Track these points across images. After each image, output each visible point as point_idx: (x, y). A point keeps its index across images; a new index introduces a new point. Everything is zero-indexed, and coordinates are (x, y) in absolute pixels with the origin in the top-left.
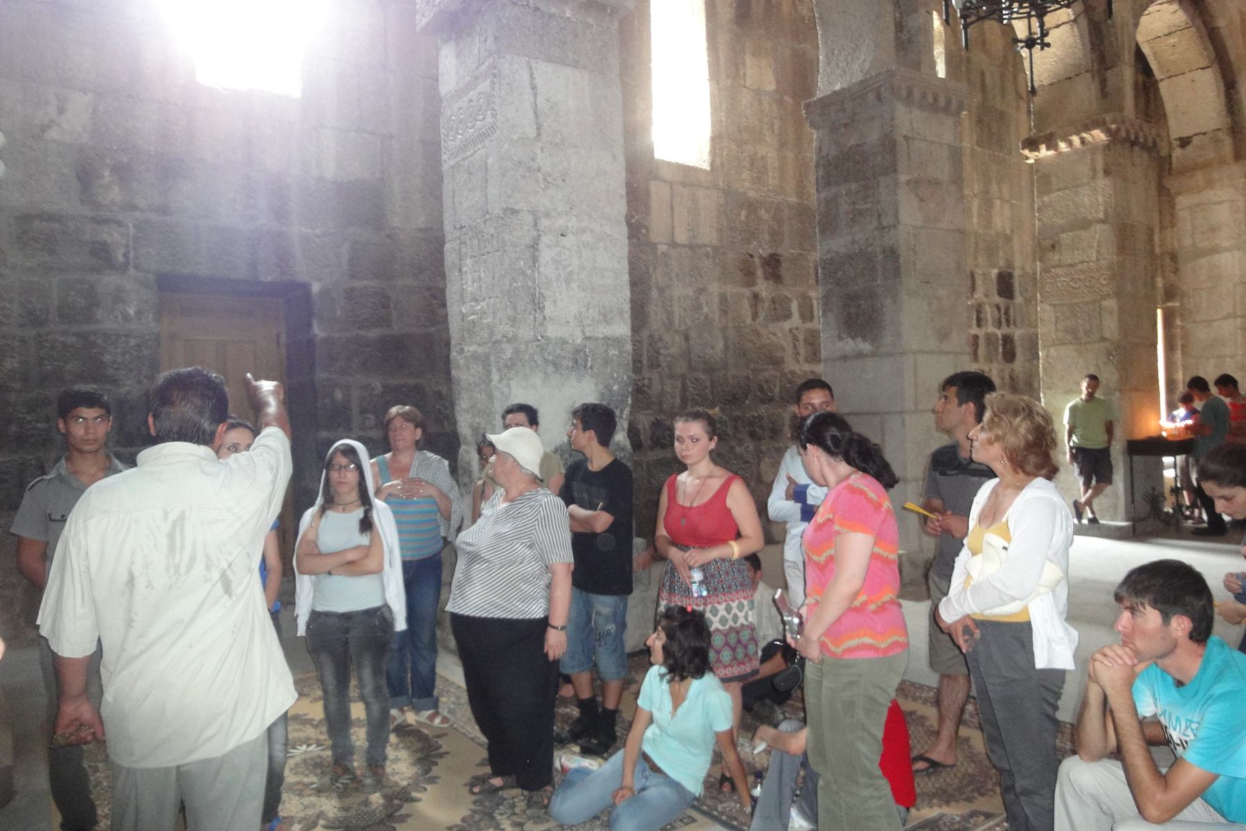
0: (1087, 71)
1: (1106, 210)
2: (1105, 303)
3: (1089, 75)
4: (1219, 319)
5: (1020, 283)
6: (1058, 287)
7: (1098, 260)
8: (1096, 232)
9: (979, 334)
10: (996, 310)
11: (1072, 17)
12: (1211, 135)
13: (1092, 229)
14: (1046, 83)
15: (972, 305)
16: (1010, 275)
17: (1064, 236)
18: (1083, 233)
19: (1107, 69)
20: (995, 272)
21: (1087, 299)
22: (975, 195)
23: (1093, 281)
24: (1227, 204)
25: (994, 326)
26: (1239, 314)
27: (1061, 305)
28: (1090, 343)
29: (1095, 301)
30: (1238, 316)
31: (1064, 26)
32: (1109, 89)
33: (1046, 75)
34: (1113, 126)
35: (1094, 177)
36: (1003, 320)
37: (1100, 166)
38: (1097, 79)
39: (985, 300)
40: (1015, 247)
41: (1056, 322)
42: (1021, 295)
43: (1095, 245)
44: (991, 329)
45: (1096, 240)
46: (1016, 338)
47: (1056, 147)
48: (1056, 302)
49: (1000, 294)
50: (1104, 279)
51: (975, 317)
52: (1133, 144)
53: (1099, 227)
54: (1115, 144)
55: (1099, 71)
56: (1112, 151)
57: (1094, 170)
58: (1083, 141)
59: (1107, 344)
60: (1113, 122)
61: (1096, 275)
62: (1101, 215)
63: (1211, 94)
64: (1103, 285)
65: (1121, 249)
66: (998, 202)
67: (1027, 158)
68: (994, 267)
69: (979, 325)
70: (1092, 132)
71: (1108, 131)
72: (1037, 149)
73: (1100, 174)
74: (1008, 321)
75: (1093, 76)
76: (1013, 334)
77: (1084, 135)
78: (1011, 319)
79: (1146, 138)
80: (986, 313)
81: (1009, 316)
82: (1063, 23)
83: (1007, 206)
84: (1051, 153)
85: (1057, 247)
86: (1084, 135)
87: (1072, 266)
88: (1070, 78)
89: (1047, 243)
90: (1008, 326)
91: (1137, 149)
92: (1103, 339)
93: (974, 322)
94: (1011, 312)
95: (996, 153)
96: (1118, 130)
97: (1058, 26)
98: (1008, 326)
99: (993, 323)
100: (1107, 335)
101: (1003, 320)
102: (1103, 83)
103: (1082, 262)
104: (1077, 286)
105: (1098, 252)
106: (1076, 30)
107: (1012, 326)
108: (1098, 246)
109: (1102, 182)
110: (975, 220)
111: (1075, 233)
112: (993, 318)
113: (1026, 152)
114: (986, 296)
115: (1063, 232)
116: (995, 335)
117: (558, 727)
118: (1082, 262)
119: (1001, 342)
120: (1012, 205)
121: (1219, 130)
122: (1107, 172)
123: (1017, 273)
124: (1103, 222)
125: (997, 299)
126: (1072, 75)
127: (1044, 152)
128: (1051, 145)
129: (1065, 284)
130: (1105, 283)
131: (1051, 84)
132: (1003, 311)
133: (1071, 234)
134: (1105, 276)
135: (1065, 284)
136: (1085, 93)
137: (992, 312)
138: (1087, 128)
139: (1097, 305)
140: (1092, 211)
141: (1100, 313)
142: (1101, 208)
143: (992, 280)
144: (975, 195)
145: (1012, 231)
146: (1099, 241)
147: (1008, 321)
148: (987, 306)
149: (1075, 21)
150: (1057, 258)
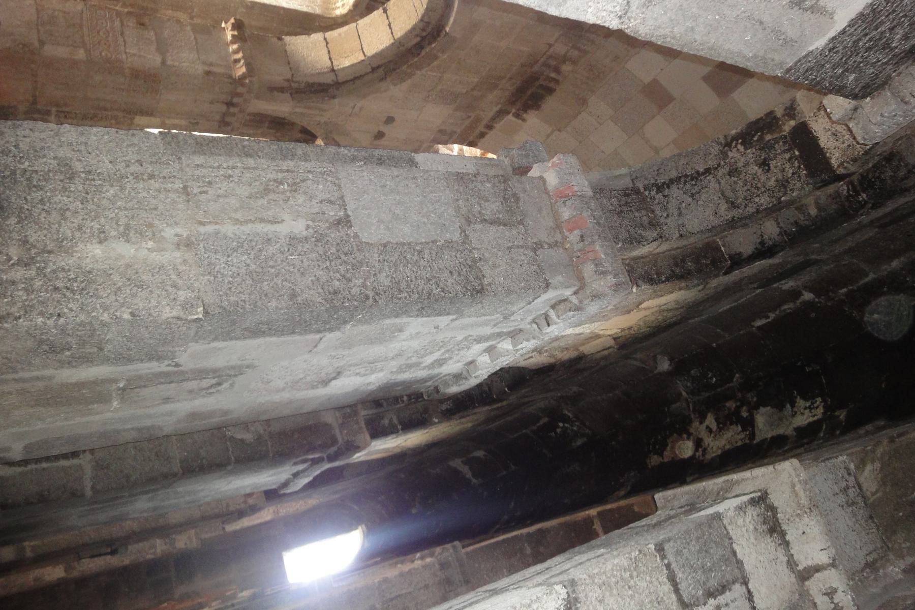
0: (293, 75)
3: (289, 76)
11: (336, 68)
14: (288, 48)
17: (152, 33)
18: (153, 48)
19: (291, 94)
29: (83, 43)
31: (330, 62)
32: (275, 93)
33: (293, 48)
34: (247, 81)
35: (204, 63)
37: (214, 69)
38: (285, 84)
45: (145, 55)
47: (233, 42)
52: (230, 104)
53: (159, 59)
54: (231, 84)
55: (290, 88)
56: (226, 80)
57: (211, 64)
58: (237, 61)
60: (250, 82)
61: (111, 49)
64: (101, 54)
65: (136, 74)
67: (226, 23)
70: (244, 67)
71: (243, 77)
72: (233, 29)
73: (207, 68)
75: (287, 80)
77: (242, 61)
79: (234, 115)
82: (332, 63)
84: (229, 38)
86: (242, 61)
87: (122, 34)
88: (289, 64)
89: (146, 20)
91: (224, 108)
92: (42, 43)
96: (243, 85)
97: (330, 58)
100: (46, 47)
102: (282, 90)
103: (124, 41)
105: (134, 55)
106: (326, 70)
109: (200, 69)
113: (232, 20)
117: (876, 118)
122: (208, 73)
124: (164, 62)
126: (291, 65)
127: (229, 35)
128: (235, 39)
131: (286, 51)
136: (277, 74)
138: (247, 64)
146: (145, 57)
149: (333, 70)
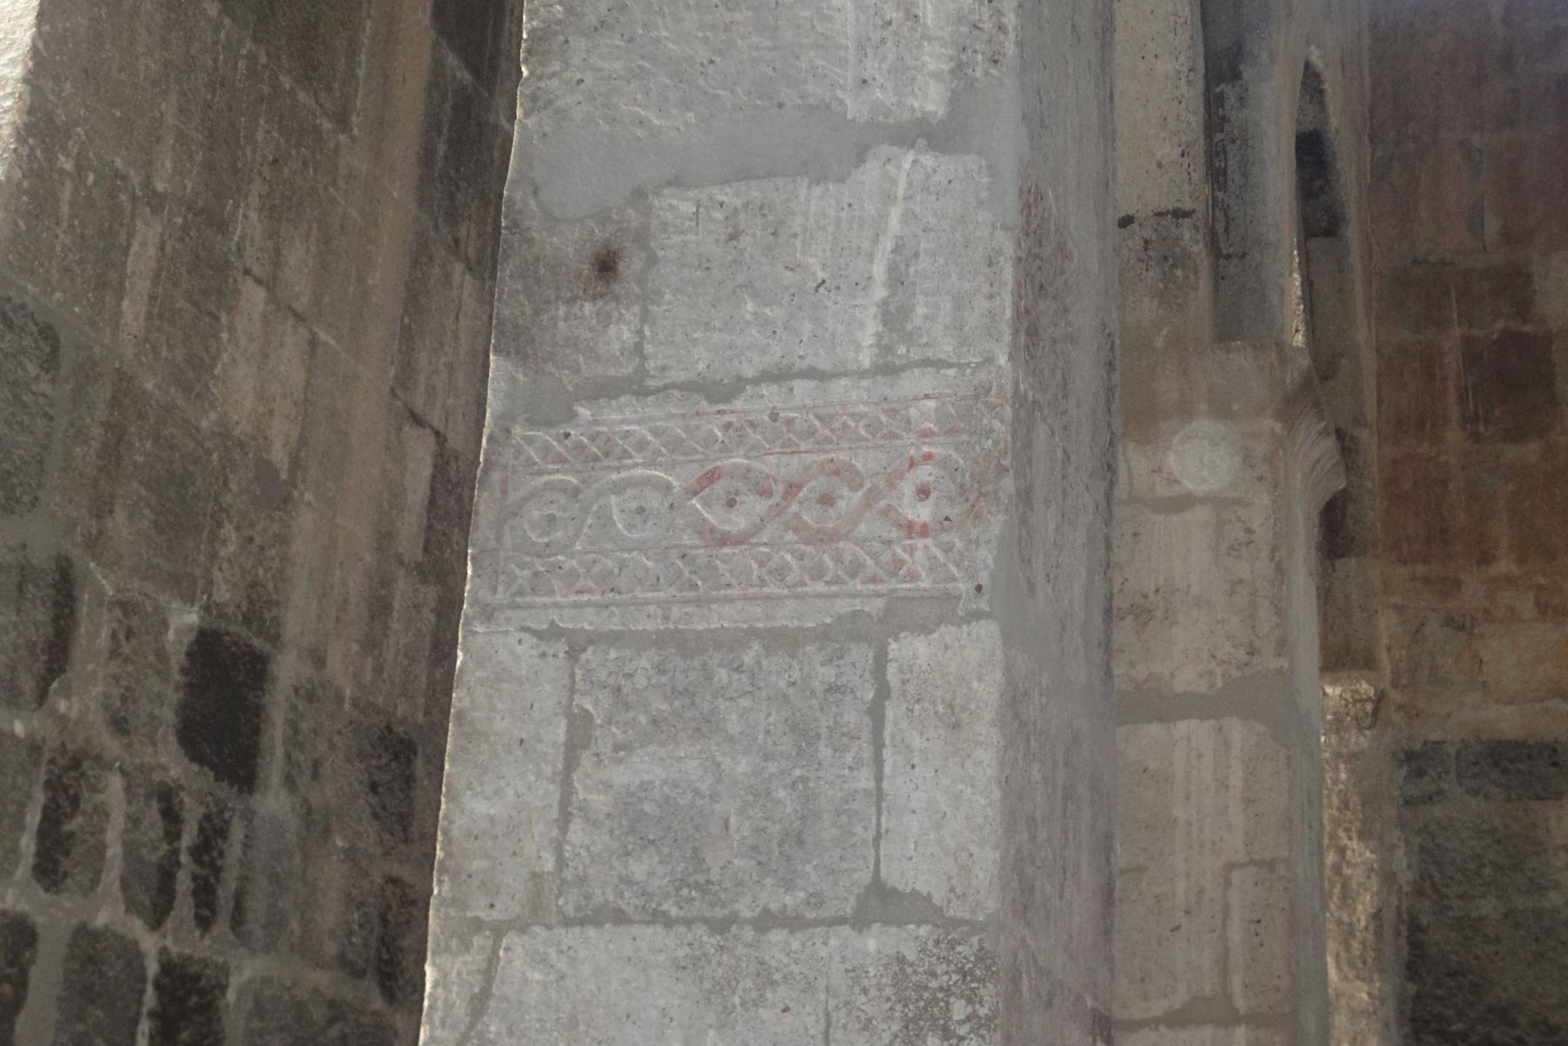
1: (959, 69)
2: (910, 650)
4: (1154, 1023)
5: (293, 725)
6: (605, 521)
7: (887, 369)
8: (889, 198)
9: (39, 920)
10: (153, 814)
12: (1148, 233)
13: (871, 172)
15: (34, 747)
16: (257, 668)
20: (185, 619)
21: (785, 617)
22: (157, 202)
23: (849, 500)
24: (1201, 514)
25: (132, 906)
26: (1241, 1004)
27: (614, 639)
28: (794, 923)
30: (1237, 1020)
36: (183, 883)
39: (111, 745)
40: (298, 546)
41: (571, 763)
42: (290, 782)
43: (879, 271)
44: (108, 914)
46: (235, 982)
48: (588, 622)
49: (192, 738)
50: (923, 492)
51: (33, 818)
53: (908, 163)
59: (908, 940)
62: (932, 100)
63: (1165, 67)
64: (912, 530)
66: (254, 298)
68: (190, 599)
69: (49, 871)
74: (204, 894)
76: (225, 970)
78: (224, 896)
80: (103, 813)
81: (217, 871)
83: (291, 340)
85: (631, 265)
87: (718, 391)
90: (204, 923)
93: (28, 844)
94: (233, 849)
95: (287, 82)
98: (204, 923)
99: (125, 886)
101: (183, 883)
103: (780, 375)
104: (738, 522)
105: (894, 317)
107: (221, 926)
108: (896, 279)
110: (132, 312)
111: (755, 192)
112: (130, 849)
114: (119, 725)
115: (676, 182)
116: (131, 953)
118: (780, 375)
119: (150, 999)
120: (313, 343)
121: (1179, 214)
123: (287, 669)
125: (171, 763)
129: (654, 501)
130: (923, 513)
132: (188, 839)
133: (725, 195)
134: (925, 473)
135: (654, 501)
137: (134, 821)
139: (861, 655)
140: (871, 67)
141: (876, 713)
142: (934, 59)
143: (161, 654)
144: (157, 202)
145: (296, 463)
146: (903, 255)
147: (204, 894)
148: (115, 783)
150: (621, 334)
